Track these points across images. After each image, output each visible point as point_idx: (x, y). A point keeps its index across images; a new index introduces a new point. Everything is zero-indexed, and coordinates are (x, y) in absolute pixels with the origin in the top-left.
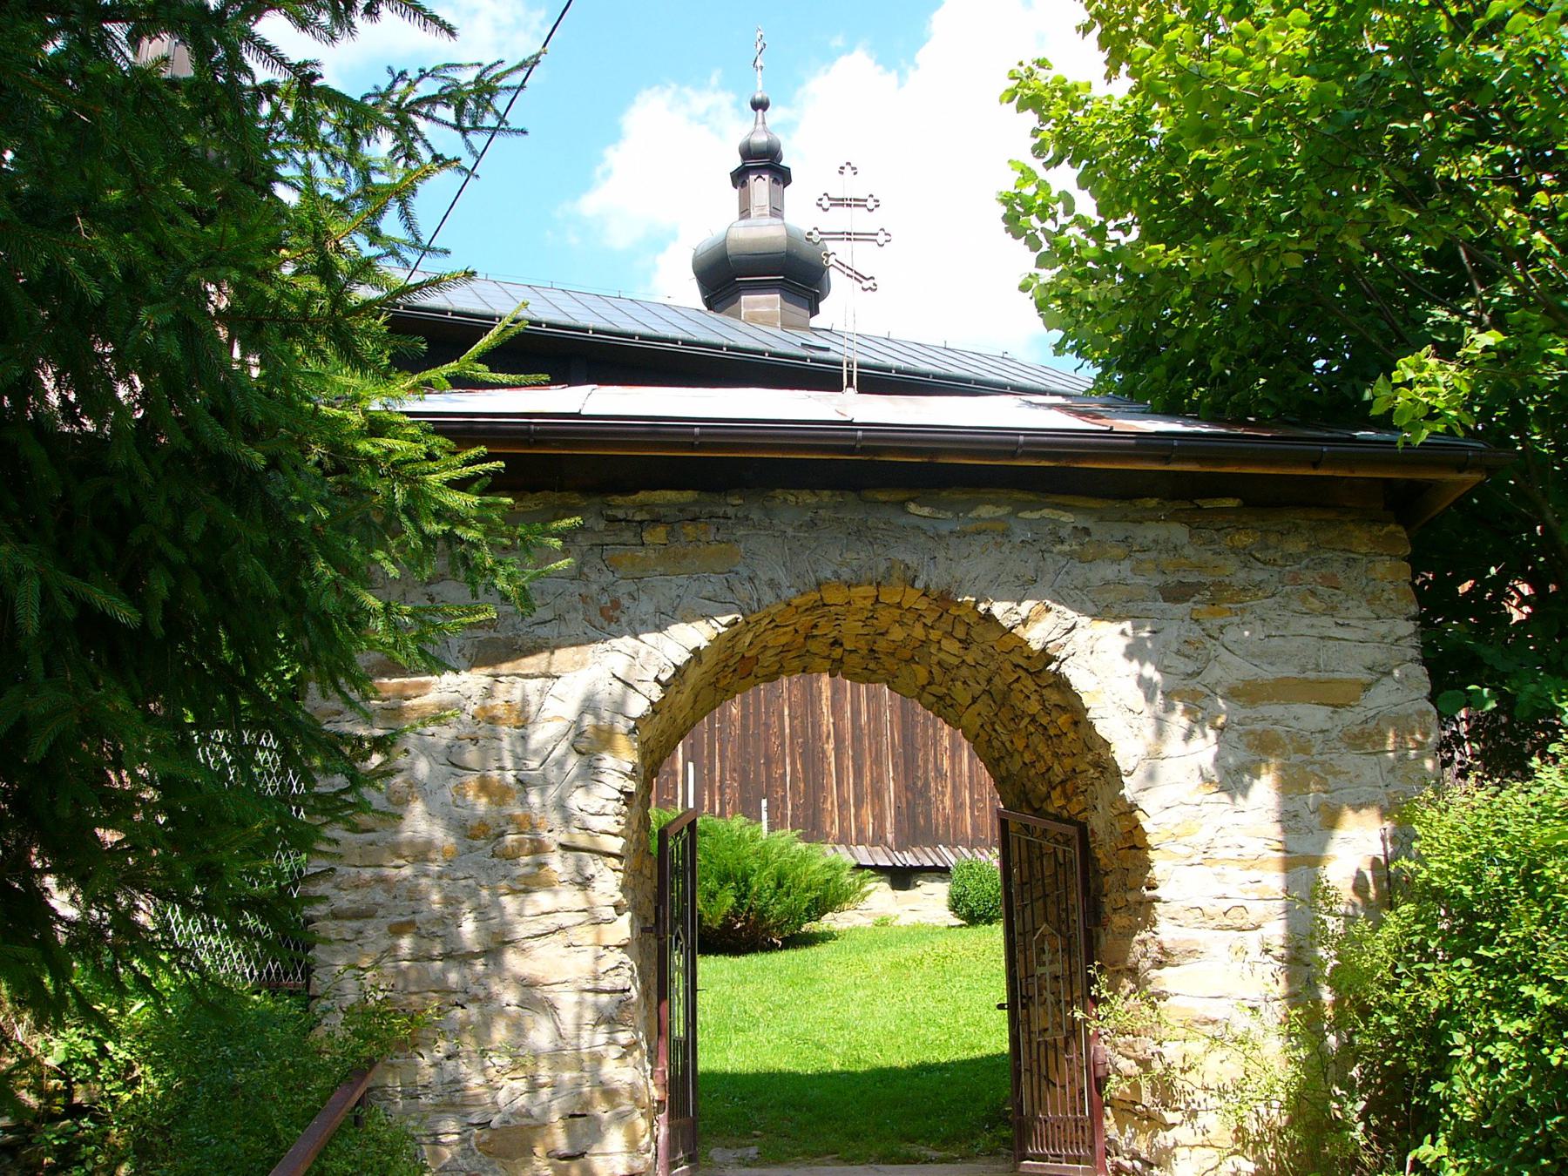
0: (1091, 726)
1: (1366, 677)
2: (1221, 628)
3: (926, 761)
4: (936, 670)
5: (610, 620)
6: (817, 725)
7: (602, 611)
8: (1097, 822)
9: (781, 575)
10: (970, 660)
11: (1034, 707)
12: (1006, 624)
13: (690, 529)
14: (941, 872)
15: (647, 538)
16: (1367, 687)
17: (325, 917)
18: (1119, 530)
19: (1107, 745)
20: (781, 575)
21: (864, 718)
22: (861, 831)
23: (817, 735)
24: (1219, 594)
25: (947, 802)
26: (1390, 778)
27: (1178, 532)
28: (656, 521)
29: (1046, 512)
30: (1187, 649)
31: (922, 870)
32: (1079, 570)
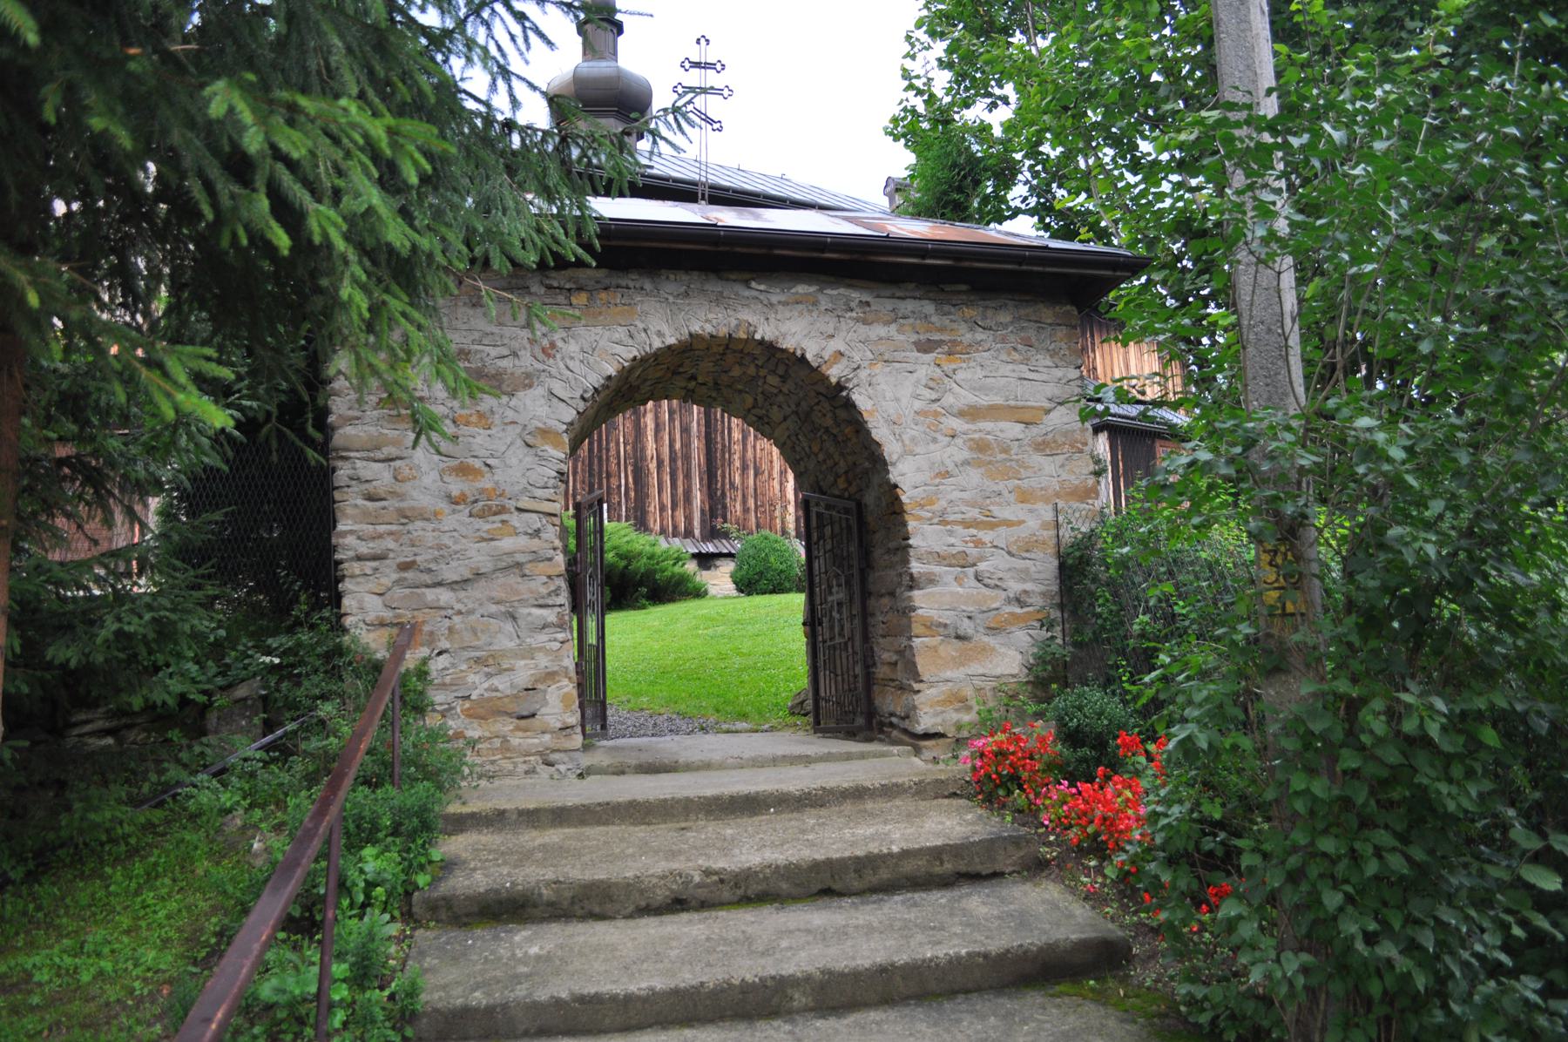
0: (868, 433)
1: (1047, 405)
2: (954, 371)
3: (723, 477)
4: (760, 398)
5: (549, 356)
6: (643, 449)
7: (543, 350)
8: (869, 499)
9: (665, 328)
10: (785, 390)
11: (829, 422)
12: (815, 364)
13: (603, 295)
14: (730, 555)
15: (574, 301)
16: (1048, 412)
17: (352, 559)
18: (889, 304)
19: (879, 445)
20: (665, 328)
21: (678, 445)
22: (675, 527)
23: (643, 458)
24: (954, 349)
25: (738, 507)
26: (1060, 471)
27: (929, 308)
28: (580, 289)
29: (842, 291)
30: (932, 384)
31: (720, 555)
32: (862, 329)
